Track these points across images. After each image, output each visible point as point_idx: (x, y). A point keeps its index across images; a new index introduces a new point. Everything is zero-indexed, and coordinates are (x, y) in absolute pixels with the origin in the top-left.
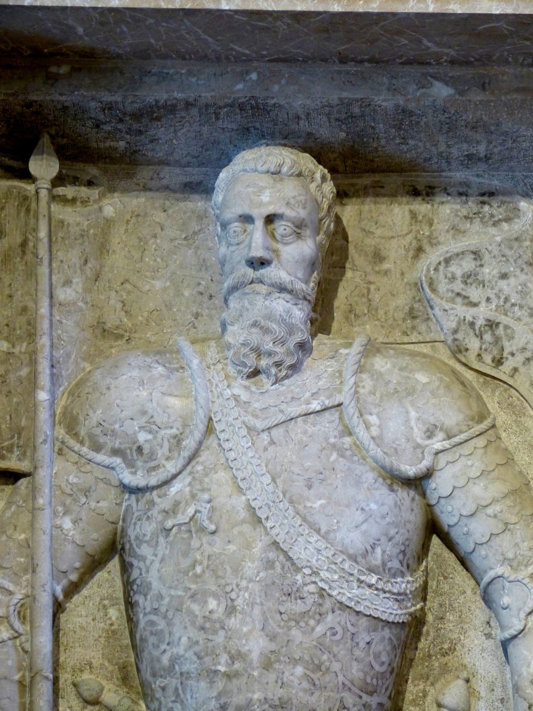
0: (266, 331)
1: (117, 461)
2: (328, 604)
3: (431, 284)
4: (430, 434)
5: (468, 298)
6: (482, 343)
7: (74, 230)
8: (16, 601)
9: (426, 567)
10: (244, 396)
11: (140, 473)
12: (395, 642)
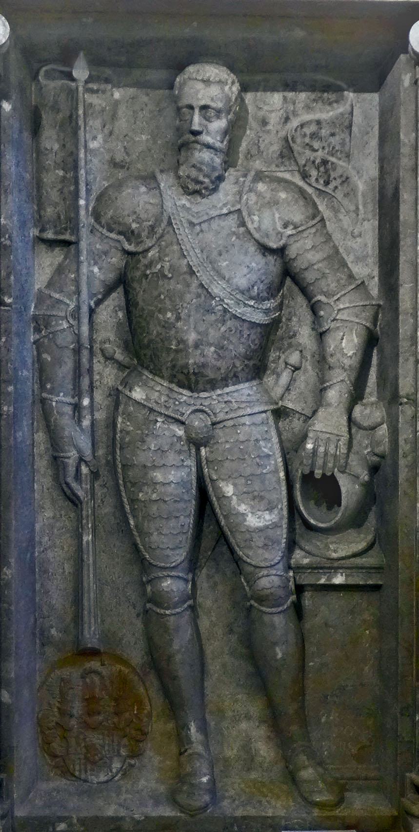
0: (200, 170)
1: (121, 238)
2: (228, 316)
3: (292, 138)
4: (285, 226)
5: (312, 146)
6: (319, 172)
7: (98, 108)
8: (70, 309)
9: (283, 293)
10: (188, 205)
11: (133, 245)
12: (263, 333)
